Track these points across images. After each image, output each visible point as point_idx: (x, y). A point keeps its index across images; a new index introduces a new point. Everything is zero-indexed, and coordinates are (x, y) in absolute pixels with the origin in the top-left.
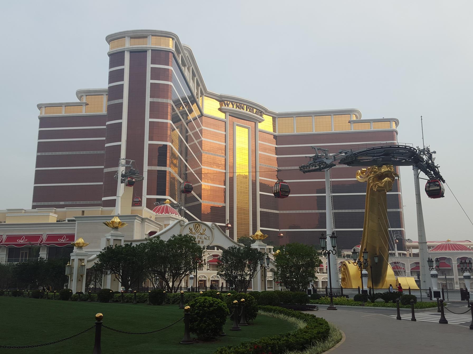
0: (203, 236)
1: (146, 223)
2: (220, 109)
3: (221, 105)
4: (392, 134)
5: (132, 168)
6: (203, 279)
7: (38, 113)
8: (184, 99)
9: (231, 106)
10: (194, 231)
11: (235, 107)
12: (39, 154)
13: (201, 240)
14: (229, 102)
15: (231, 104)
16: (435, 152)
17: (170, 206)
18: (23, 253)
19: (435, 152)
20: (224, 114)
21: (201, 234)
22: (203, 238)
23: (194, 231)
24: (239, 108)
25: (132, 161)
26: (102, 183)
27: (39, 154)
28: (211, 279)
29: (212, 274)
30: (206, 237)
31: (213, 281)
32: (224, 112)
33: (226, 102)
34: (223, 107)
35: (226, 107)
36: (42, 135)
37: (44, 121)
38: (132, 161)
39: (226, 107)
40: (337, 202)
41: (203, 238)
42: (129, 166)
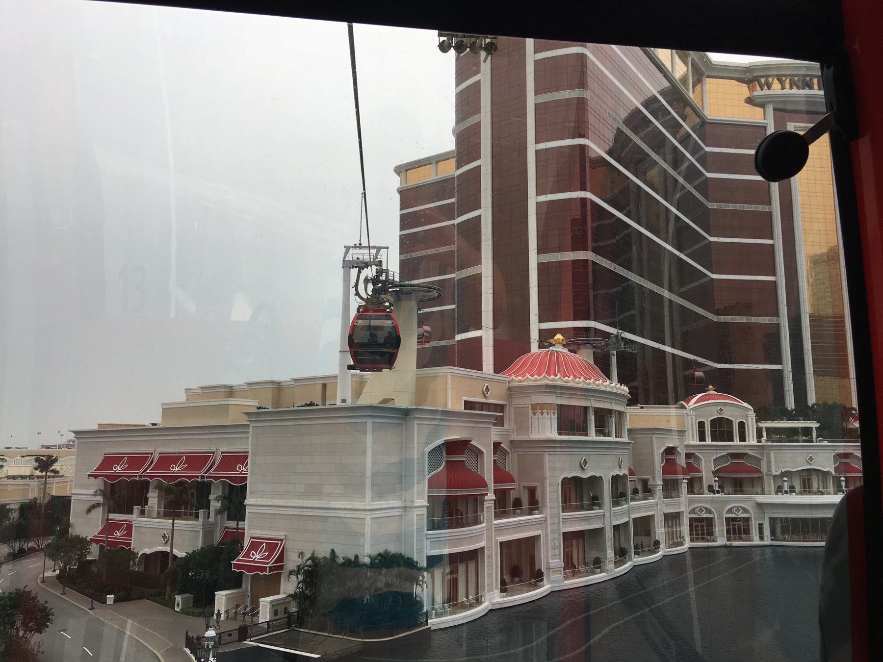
1: (416, 422)
2: (750, 101)
3: (751, 89)
4: (831, 257)
6: (704, 515)
7: (396, 182)
8: (651, 103)
9: (776, 85)
11: (787, 86)
14: (770, 80)
15: (776, 81)
16: (46, 602)
17: (565, 351)
19: (46, 602)
20: (759, 110)
24: (798, 88)
26: (454, 306)
28: (725, 515)
32: (762, 105)
33: (763, 80)
34: (755, 93)
35: (766, 92)
36: (406, 221)
37: (407, 197)
39: (766, 92)
40: (720, 431)
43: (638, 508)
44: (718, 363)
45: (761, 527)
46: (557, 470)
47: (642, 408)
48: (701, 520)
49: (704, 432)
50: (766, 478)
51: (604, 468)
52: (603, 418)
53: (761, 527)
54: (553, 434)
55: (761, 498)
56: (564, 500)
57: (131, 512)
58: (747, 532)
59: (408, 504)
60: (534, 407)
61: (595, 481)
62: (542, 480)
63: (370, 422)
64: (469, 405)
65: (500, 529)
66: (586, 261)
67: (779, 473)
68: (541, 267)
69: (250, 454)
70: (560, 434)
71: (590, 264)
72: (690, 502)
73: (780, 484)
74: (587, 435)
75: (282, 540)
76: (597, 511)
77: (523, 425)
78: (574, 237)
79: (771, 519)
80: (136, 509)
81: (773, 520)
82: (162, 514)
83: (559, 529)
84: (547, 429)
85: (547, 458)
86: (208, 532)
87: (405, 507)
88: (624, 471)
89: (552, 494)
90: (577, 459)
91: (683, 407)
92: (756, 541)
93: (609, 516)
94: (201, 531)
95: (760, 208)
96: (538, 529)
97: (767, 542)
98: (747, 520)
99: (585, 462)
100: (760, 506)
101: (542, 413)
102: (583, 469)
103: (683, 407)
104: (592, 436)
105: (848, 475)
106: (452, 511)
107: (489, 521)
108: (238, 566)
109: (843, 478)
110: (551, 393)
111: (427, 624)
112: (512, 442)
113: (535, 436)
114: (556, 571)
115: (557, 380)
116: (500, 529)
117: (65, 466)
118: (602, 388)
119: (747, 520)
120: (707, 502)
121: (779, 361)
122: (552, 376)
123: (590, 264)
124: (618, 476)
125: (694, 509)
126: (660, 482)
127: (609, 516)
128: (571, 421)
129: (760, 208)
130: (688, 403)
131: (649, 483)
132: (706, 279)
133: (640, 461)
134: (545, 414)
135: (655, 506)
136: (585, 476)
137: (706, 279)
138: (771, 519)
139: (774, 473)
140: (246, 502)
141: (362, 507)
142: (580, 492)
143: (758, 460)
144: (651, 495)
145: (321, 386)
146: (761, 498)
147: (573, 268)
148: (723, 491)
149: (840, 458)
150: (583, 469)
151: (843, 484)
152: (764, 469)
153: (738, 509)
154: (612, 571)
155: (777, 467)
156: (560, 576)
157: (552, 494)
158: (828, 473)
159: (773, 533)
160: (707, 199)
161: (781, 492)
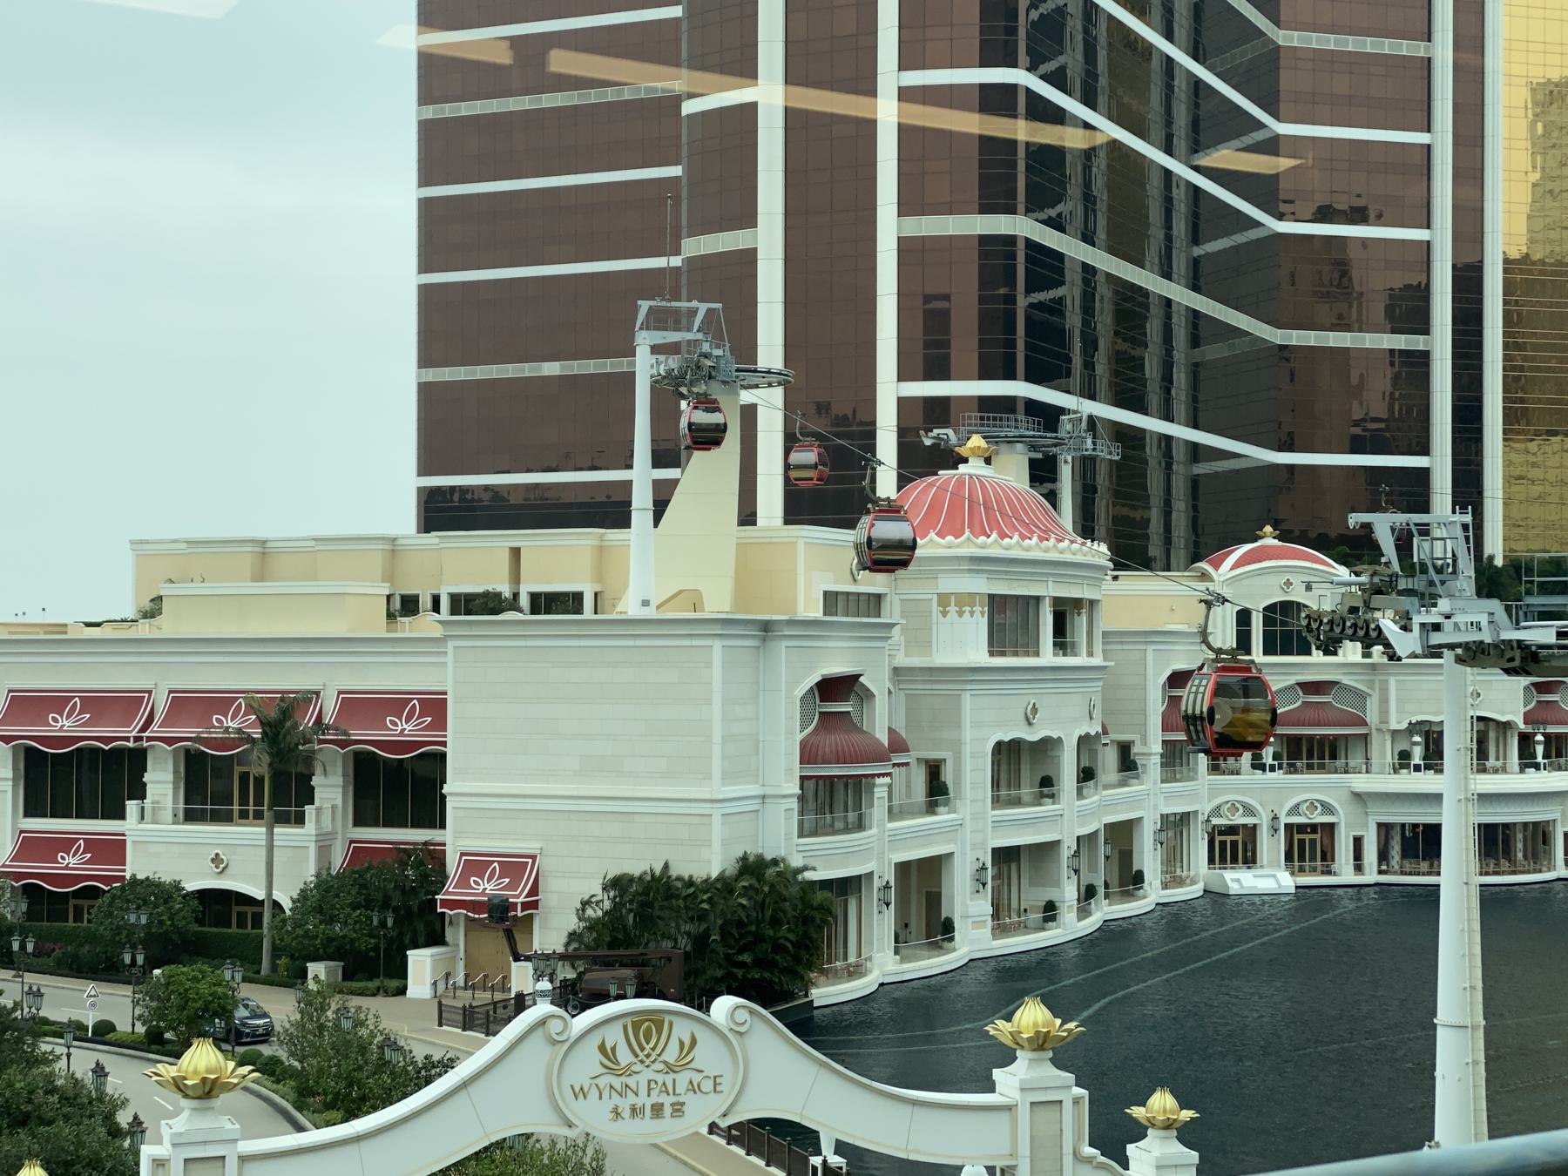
0: (683, 1079)
1: (784, 643)
5: (706, 347)
6: (1240, 820)
10: (624, 1056)
12: (430, 112)
13: (667, 1100)
18: (244, 777)
21: (670, 1068)
22: (682, 1086)
23: (624, 1056)
25: (703, 308)
27: (430, 112)
29: (1294, 790)
30: (697, 1078)
31: (1302, 828)
38: (703, 308)
41: (682, 1086)
42: (689, 336)
43: (1109, 803)
44: (1280, 450)
45: (1358, 841)
46: (981, 727)
47: (1115, 578)
48: (1232, 830)
49: (1249, 633)
50: (1375, 740)
51: (1065, 721)
52: (1064, 613)
53: (1358, 841)
54: (978, 654)
55: (1360, 782)
56: (996, 784)
57: (120, 815)
58: (1328, 855)
59: (769, 791)
60: (944, 600)
61: (1047, 747)
62: (957, 746)
63: (718, 645)
64: (831, 600)
65: (895, 840)
66: (1011, 240)
67: (1404, 725)
68: (907, 248)
69: (450, 698)
70: (991, 654)
71: (1021, 245)
72: (1213, 792)
73: (1404, 746)
74: (1037, 654)
75: (534, 858)
76: (1048, 808)
77: (921, 638)
78: (984, 182)
79: (1379, 825)
80: (132, 806)
81: (1385, 829)
82: (181, 815)
83: (985, 842)
84: (965, 641)
85: (967, 700)
86: (323, 850)
87: (764, 797)
88: (1095, 728)
89: (972, 775)
90: (1018, 706)
91: (1204, 576)
92: (1345, 874)
93: (1070, 817)
94: (312, 846)
95: (1405, 48)
96: (949, 842)
97: (1371, 876)
98: (1330, 828)
99: (1035, 710)
100: (1359, 797)
101: (961, 614)
102: (1030, 724)
103: (1204, 576)
104: (1048, 656)
105: (1551, 729)
106: (831, 799)
107: (881, 825)
108: (445, 903)
109: (1539, 738)
110: (978, 571)
111: (806, 995)
112: (896, 671)
113: (942, 658)
114: (978, 924)
115: (991, 546)
116: (895, 840)
117: (1389, 758)
118: (1068, 557)
119: (1330, 828)
120: (1243, 791)
121: (1425, 451)
122: (983, 538)
123: (1021, 245)
124: (1087, 735)
125: (1297, 806)
126: (1157, 748)
127: (1070, 817)
128: (1010, 621)
129: (1405, 48)
130: (1217, 567)
131: (1135, 750)
132: (1253, 234)
133: (1116, 701)
134: (967, 615)
135: (1148, 799)
136: (1033, 736)
137: (1253, 234)
138: (1379, 825)
139: (1394, 726)
140: (446, 789)
141: (708, 796)
142: (1021, 766)
143: (1361, 697)
144: (1137, 777)
145: (505, 557)
146: (1360, 782)
147: (983, 255)
148: (1280, 767)
149: (1539, 692)
150: (1030, 724)
151: (1540, 750)
152: (1372, 717)
153: (1312, 807)
154: (1071, 927)
155: (1400, 711)
156: (987, 931)
157: (972, 775)
158: (1505, 727)
159: (1383, 856)
160: (1277, 24)
161: (1407, 766)
